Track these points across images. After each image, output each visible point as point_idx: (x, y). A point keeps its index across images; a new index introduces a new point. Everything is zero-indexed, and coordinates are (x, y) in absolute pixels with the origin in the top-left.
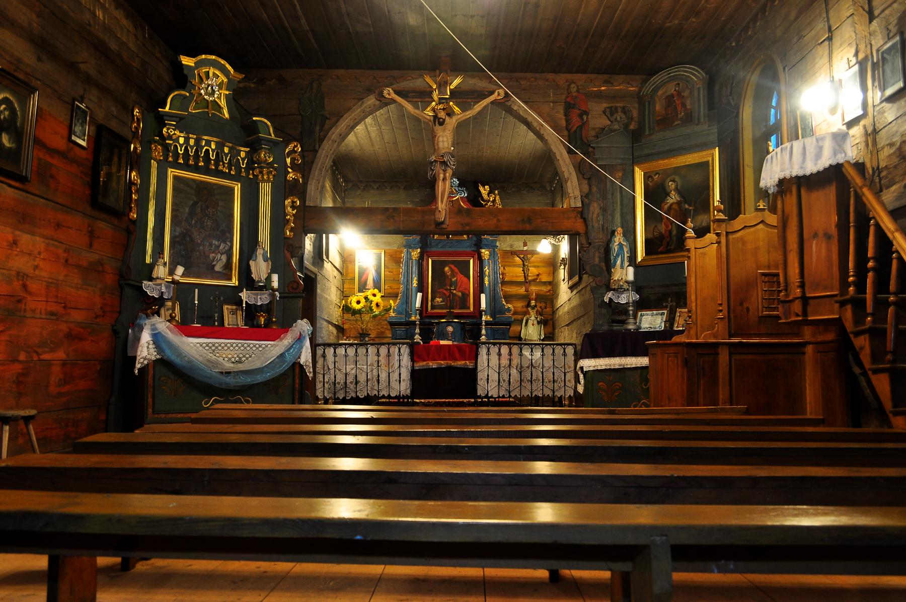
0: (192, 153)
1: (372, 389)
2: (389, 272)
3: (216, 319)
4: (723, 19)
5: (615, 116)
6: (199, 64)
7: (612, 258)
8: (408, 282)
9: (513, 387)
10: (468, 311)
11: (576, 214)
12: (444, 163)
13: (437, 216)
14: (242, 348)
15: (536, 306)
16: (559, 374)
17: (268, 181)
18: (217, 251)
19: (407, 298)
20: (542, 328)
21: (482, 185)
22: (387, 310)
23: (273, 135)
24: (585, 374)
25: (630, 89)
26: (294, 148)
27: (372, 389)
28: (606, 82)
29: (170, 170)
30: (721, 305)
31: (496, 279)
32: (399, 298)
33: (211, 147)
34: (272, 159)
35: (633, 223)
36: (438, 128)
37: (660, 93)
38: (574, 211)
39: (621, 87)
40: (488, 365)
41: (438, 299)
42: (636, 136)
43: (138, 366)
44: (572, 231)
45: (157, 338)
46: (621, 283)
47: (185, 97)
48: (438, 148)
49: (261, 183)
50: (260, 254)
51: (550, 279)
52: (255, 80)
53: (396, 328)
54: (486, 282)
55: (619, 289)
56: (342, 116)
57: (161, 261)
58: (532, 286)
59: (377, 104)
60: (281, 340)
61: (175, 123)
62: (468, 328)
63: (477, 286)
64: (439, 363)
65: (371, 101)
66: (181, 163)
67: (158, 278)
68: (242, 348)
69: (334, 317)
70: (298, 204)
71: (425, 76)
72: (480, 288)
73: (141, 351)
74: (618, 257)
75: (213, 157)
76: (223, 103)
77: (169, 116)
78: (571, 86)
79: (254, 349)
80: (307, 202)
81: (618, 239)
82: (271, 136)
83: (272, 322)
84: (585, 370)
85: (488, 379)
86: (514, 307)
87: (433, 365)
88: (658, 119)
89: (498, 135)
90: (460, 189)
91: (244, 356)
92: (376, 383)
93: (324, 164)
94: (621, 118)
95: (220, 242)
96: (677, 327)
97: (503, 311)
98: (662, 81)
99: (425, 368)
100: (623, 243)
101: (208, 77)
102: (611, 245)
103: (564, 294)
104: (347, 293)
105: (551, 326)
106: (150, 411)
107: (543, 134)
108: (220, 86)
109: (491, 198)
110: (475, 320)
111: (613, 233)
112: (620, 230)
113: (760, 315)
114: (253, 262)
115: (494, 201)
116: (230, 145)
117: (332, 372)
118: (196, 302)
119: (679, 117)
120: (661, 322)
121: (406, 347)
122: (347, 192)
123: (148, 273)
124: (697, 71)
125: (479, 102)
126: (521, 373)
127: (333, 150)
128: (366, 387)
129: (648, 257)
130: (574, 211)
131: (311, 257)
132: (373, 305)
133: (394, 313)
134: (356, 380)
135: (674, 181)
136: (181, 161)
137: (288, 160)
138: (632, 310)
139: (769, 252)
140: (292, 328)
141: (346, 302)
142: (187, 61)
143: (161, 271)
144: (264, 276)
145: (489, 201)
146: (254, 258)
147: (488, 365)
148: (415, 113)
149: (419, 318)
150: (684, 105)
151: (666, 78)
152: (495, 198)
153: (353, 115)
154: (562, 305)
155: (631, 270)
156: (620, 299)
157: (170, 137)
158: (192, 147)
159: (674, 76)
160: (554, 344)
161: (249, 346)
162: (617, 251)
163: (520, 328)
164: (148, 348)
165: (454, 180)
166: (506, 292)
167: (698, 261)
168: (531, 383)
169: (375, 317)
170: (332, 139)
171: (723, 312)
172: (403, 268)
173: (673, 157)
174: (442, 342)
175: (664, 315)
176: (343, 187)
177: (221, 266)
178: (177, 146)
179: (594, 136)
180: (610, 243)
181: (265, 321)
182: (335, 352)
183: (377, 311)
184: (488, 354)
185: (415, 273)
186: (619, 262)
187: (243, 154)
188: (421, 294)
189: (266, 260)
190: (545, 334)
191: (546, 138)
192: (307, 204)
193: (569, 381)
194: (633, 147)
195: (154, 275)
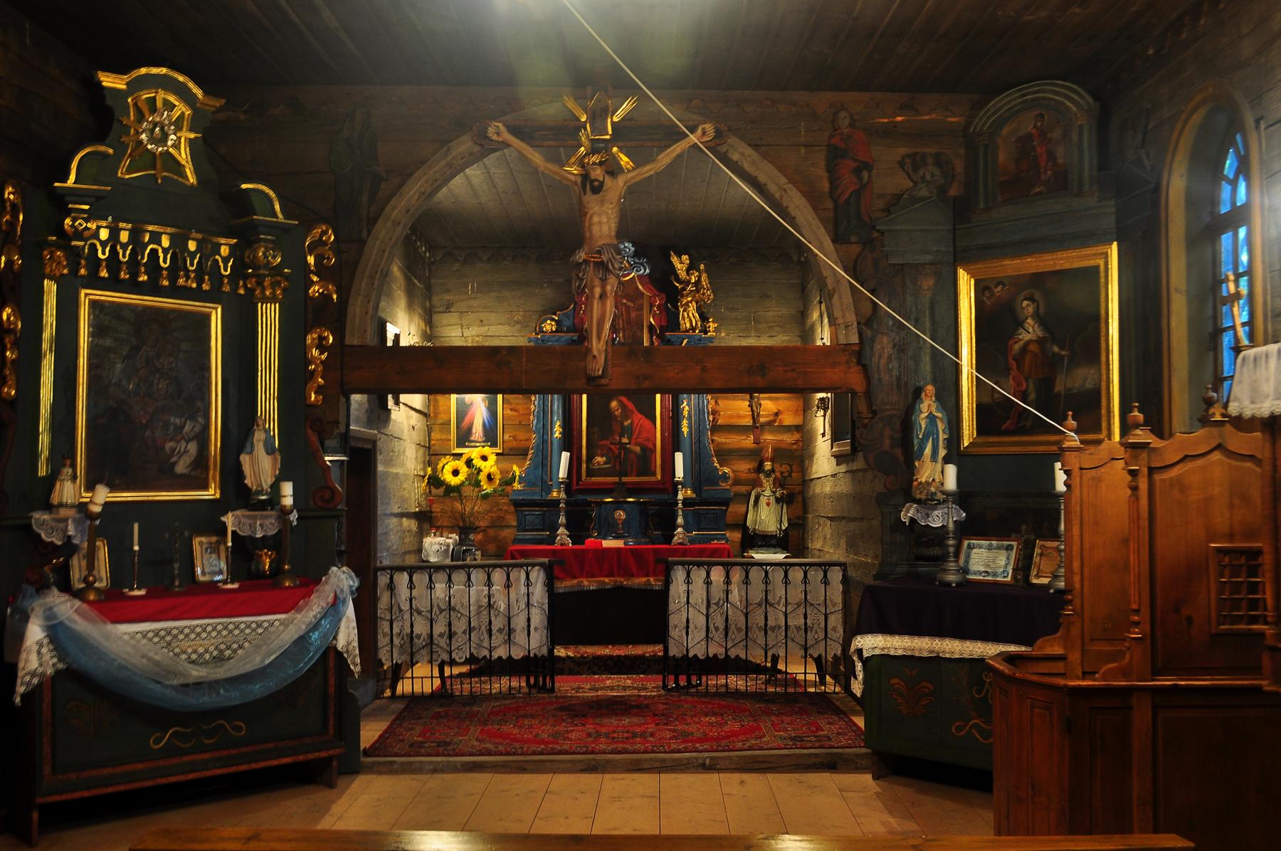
0: (124, 256)
1: (479, 646)
2: (511, 409)
3: (176, 572)
4: (1134, 9)
5: (921, 173)
6: (135, 86)
7: (916, 442)
8: (545, 429)
9: (733, 640)
10: (653, 479)
11: (847, 357)
12: (602, 266)
13: (589, 367)
14: (225, 633)
15: (773, 471)
16: (815, 618)
17: (273, 299)
18: (179, 437)
19: (544, 457)
20: (785, 510)
21: (676, 254)
22: (508, 482)
23: (280, 215)
24: (866, 662)
25: (949, 119)
26: (321, 236)
27: (479, 646)
28: (904, 107)
29: (83, 292)
30: (1137, 611)
31: (700, 422)
32: (529, 457)
33: (160, 245)
34: (280, 259)
35: (954, 372)
36: (590, 199)
37: (1005, 131)
38: (843, 350)
39: (934, 116)
40: (688, 602)
41: (599, 459)
42: (961, 210)
43: (21, 689)
44: (841, 388)
45: (56, 633)
46: (933, 489)
47: (106, 155)
48: (591, 236)
49: (260, 305)
50: (260, 440)
51: (797, 421)
52: (246, 107)
53: (525, 511)
54: (685, 430)
55: (929, 500)
56: (412, 174)
57: (68, 471)
58: (766, 434)
59: (475, 151)
60: (299, 611)
61: (87, 207)
62: (652, 510)
63: (669, 435)
64: (600, 581)
65: (464, 145)
66: (104, 278)
67: (61, 505)
68: (225, 633)
69: (413, 501)
70: (331, 341)
71: (566, 99)
72: (673, 442)
73: (27, 661)
74: (928, 441)
75: (165, 262)
76: (183, 156)
77: (75, 195)
78: (840, 115)
79: (248, 631)
80: (347, 338)
81: (928, 406)
82: (277, 218)
83: (284, 572)
84: (866, 654)
85: (688, 627)
86: (734, 471)
87: (589, 584)
88: (1001, 179)
89: (704, 181)
90: (637, 261)
91: (228, 648)
92: (486, 636)
93: (379, 265)
94: (933, 175)
95: (183, 419)
96: (1038, 576)
97: (714, 478)
98: (1010, 109)
99: (576, 589)
100: (936, 414)
101: (153, 110)
102: (913, 418)
103: (823, 460)
104: (437, 447)
105: (801, 504)
106: (47, 769)
107: (787, 207)
108: (178, 124)
109: (693, 277)
110: (666, 497)
111: (917, 393)
112: (930, 389)
113: (1213, 631)
114: (247, 457)
115: (698, 282)
116: (199, 236)
117: (407, 616)
118: (136, 548)
119: (1043, 178)
120: (1007, 565)
121: (539, 571)
122: (434, 268)
123: (42, 494)
124: (1076, 92)
125: (670, 146)
126: (746, 615)
127: (393, 240)
128: (468, 643)
129: (981, 440)
130: (843, 350)
131: (363, 411)
132: (482, 477)
133: (520, 483)
134: (450, 630)
135: (1031, 299)
136: (104, 274)
137: (311, 260)
138: (953, 546)
139: (1231, 507)
140: (320, 587)
141: (434, 470)
142: (109, 81)
143: (68, 491)
144: (267, 481)
145: (688, 282)
146: (248, 449)
147: (688, 602)
148: (546, 168)
149: (565, 497)
150: (1052, 156)
151: (1019, 104)
152: (699, 277)
153: (431, 172)
154: (820, 478)
155: (951, 470)
156: (930, 519)
157: (79, 235)
158: (124, 247)
159: (1033, 100)
160: (805, 565)
161: (237, 627)
162: (926, 428)
163: (745, 509)
164: (39, 653)
165: (626, 245)
166: (719, 444)
167: (1085, 494)
168: (766, 633)
169: (486, 497)
170: (393, 217)
171: (1141, 626)
172: (536, 402)
173: (1031, 253)
174: (607, 543)
175: (1012, 549)
176: (427, 260)
177: (188, 463)
178: (95, 246)
179: (883, 210)
180: (912, 414)
181: (271, 563)
182: (411, 580)
183: (487, 488)
184: (688, 581)
185: (558, 413)
186: (928, 450)
187: (224, 251)
188: (569, 454)
189: (270, 451)
190: (789, 520)
191: (793, 213)
192: (347, 342)
193: (834, 629)
194: (954, 229)
195: (55, 499)
